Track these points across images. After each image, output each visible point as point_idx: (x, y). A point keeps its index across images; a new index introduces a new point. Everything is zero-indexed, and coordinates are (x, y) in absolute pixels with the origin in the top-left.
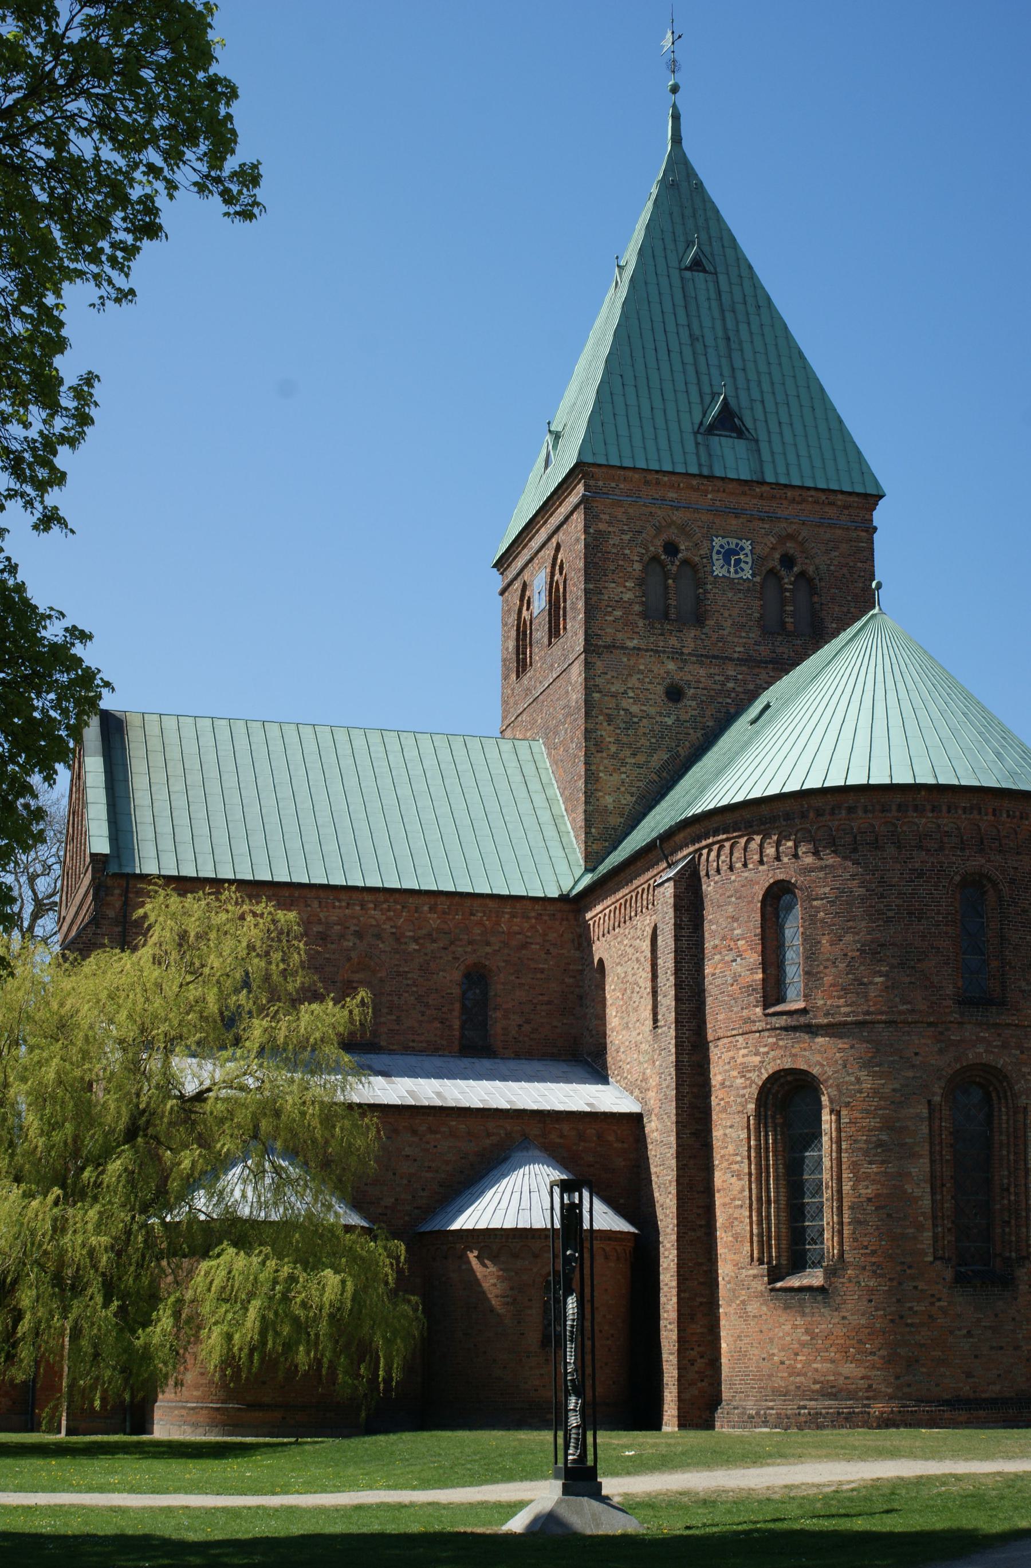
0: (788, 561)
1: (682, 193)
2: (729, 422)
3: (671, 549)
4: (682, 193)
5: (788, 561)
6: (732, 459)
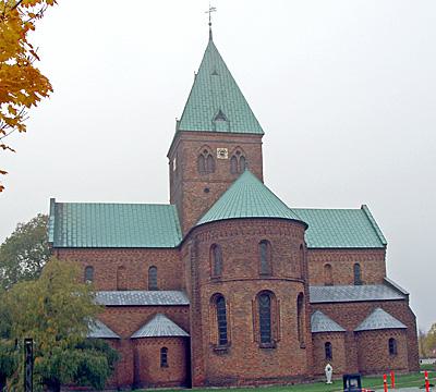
0: (238, 153)
1: (212, 52)
2: (221, 116)
3: (206, 151)
4: (212, 52)
5: (238, 153)
6: (222, 127)
